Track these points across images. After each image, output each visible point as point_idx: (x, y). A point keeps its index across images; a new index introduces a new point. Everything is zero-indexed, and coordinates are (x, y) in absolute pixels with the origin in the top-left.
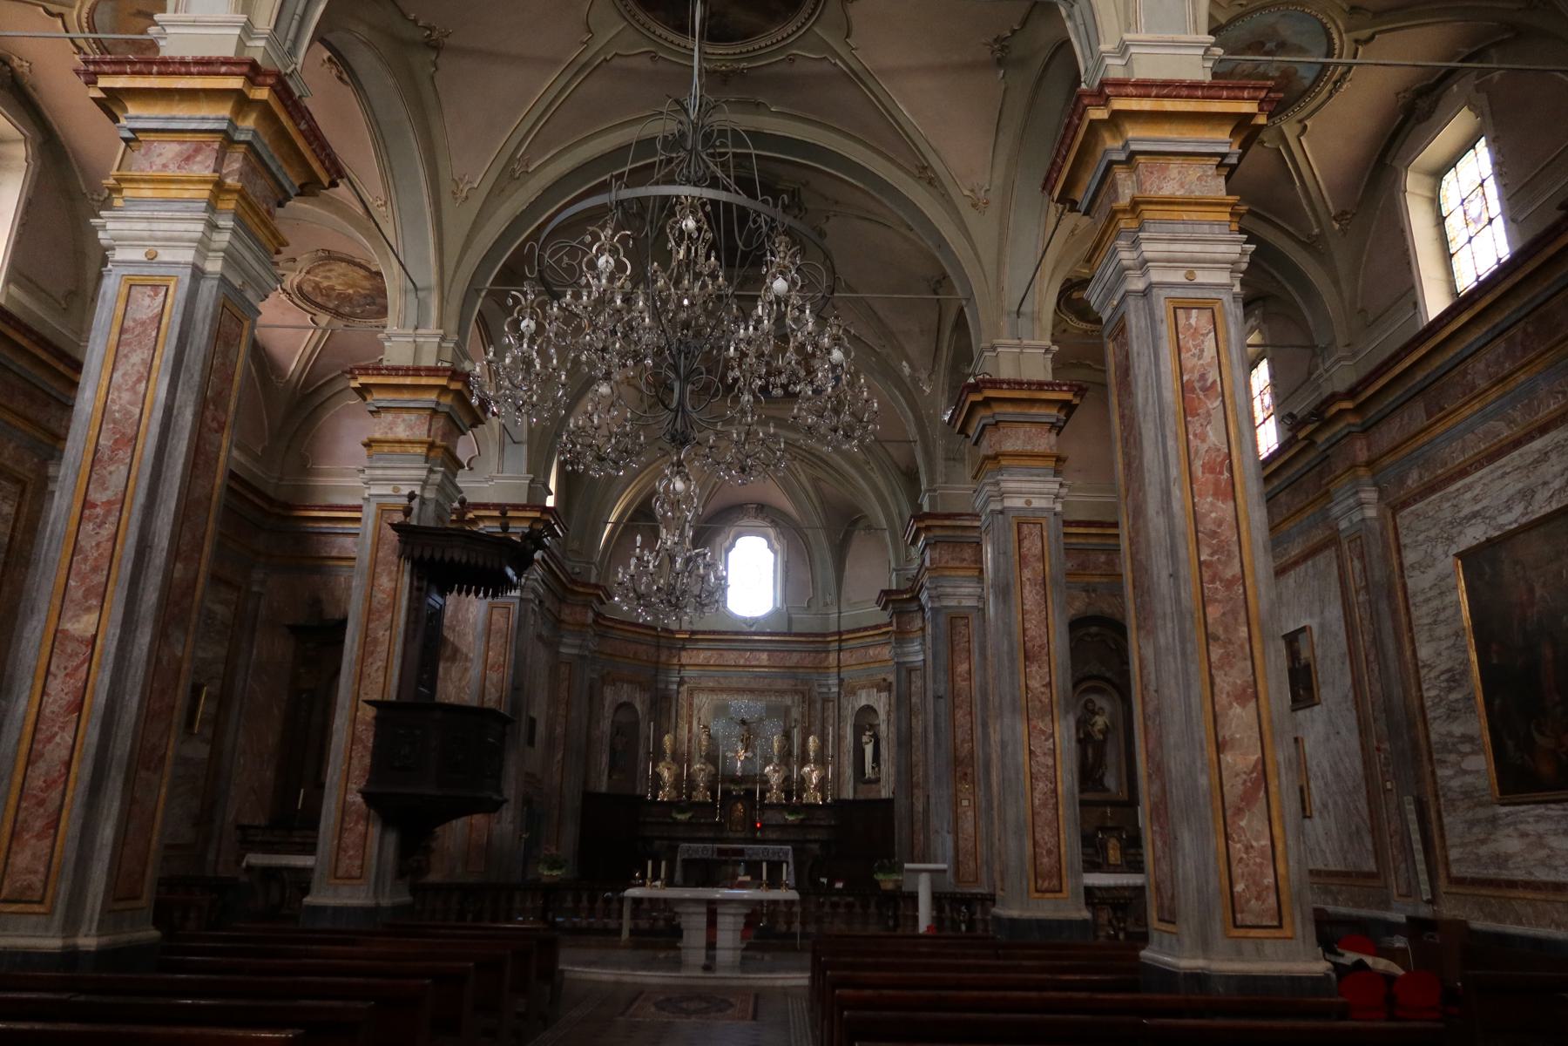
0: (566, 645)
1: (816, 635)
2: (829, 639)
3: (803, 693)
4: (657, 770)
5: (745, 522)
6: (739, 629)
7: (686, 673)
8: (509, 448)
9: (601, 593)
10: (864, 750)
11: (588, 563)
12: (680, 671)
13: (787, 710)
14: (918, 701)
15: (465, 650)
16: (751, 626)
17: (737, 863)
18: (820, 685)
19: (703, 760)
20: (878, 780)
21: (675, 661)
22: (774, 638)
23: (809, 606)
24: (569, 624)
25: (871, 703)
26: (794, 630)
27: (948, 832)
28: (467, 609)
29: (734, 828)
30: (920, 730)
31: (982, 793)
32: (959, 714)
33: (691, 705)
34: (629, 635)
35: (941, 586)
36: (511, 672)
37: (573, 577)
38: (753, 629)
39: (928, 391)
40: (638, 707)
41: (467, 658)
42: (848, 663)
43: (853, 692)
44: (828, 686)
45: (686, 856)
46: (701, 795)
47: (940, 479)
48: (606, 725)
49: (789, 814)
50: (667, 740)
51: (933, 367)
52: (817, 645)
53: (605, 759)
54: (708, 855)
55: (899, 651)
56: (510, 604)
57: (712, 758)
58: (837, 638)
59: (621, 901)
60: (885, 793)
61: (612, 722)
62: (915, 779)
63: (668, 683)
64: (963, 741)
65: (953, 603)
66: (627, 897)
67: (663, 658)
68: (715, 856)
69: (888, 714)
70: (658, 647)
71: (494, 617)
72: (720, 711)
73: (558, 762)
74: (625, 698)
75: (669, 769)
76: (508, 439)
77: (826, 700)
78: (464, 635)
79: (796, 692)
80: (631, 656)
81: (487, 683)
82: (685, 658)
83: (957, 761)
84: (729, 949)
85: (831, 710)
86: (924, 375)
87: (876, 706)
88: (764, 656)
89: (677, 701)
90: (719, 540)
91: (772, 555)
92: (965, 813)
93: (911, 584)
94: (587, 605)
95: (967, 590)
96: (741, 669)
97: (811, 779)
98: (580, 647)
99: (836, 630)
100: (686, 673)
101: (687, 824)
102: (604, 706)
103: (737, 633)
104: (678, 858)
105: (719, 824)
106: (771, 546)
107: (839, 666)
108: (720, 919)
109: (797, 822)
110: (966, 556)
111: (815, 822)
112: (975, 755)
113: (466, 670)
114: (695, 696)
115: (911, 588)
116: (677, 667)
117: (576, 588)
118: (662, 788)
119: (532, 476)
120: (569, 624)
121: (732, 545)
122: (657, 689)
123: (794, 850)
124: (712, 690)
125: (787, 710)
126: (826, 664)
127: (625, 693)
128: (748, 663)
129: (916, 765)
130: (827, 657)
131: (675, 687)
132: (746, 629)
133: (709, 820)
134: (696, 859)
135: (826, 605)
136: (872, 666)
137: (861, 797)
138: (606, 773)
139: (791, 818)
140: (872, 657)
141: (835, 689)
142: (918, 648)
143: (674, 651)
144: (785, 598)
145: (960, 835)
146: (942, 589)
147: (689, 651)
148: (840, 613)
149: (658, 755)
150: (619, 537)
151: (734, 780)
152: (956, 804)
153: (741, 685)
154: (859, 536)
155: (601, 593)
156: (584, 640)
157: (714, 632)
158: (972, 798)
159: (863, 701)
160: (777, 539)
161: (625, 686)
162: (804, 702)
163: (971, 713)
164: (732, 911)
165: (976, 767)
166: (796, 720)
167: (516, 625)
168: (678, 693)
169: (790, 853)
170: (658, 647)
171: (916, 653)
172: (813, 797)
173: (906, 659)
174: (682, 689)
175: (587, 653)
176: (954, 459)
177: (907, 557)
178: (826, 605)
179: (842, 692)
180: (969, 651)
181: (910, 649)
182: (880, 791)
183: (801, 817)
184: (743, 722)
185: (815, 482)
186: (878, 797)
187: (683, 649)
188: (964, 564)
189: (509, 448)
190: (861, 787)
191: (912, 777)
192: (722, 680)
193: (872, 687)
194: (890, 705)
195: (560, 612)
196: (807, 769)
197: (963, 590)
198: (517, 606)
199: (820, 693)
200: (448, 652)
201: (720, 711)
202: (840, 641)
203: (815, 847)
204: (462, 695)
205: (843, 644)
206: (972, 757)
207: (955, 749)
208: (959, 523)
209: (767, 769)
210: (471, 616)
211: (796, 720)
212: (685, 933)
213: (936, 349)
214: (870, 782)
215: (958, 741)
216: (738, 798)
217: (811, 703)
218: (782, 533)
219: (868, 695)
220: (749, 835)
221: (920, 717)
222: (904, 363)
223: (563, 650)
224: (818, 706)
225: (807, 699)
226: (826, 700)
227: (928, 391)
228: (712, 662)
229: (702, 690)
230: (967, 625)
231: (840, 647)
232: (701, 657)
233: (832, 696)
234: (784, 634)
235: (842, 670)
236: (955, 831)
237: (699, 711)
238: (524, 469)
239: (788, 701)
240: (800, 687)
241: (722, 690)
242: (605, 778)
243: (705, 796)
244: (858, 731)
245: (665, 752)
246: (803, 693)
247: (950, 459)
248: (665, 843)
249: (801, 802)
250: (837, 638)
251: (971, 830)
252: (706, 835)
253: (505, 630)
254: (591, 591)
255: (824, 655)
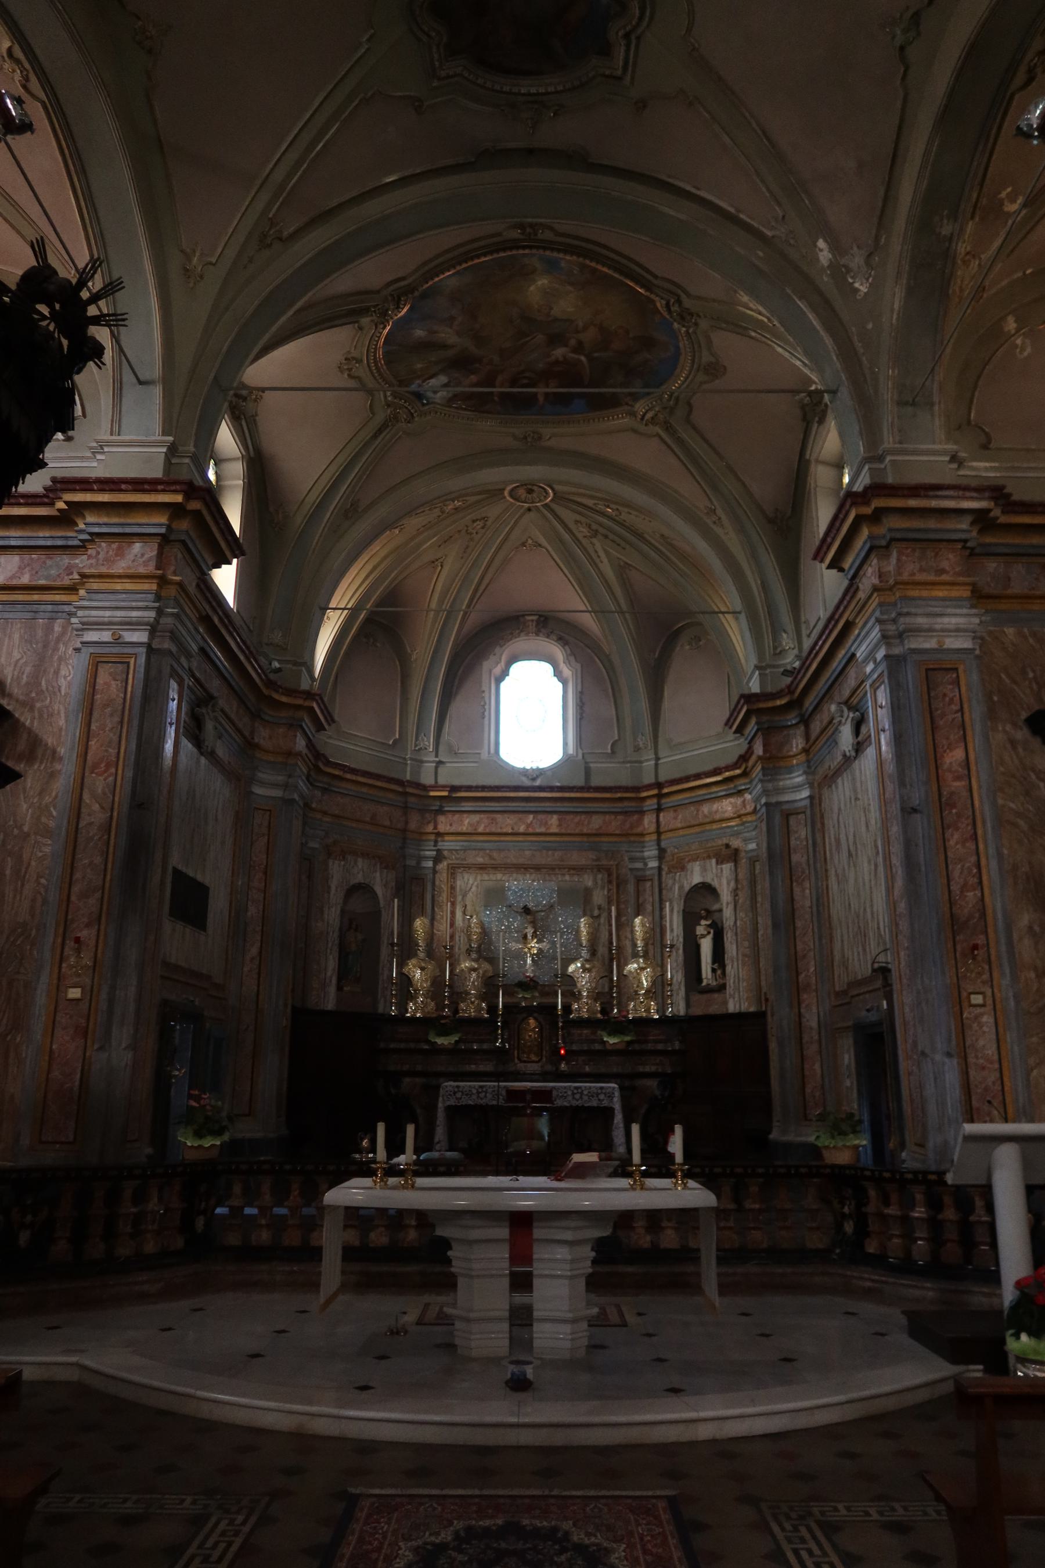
0: (263, 784)
1: (626, 789)
2: (645, 794)
3: (609, 871)
4: (405, 970)
5: (520, 643)
6: (520, 784)
7: (448, 844)
8: (132, 393)
9: (315, 705)
10: (698, 947)
11: (295, 664)
12: (436, 842)
13: (588, 893)
14: (804, 860)
15: (50, 741)
16: (534, 779)
17: (538, 1113)
18: (632, 859)
19: (474, 956)
20: (722, 988)
21: (430, 828)
22: (567, 795)
23: (613, 752)
24: (266, 751)
25: (708, 880)
26: (595, 782)
27: (949, 1055)
28: (57, 672)
29: (524, 1057)
30: (808, 903)
31: (1006, 981)
32: (954, 839)
33: (453, 888)
34: (365, 790)
35: (908, 614)
36: (130, 774)
37: (272, 676)
38: (538, 783)
39: (864, 289)
40: (379, 890)
41: (54, 756)
42: (671, 826)
43: (681, 866)
44: (643, 860)
45: (452, 1102)
46: (470, 1009)
47: (888, 441)
48: (332, 916)
49: (610, 1035)
50: (420, 925)
51: (877, 239)
52: (626, 804)
53: (331, 965)
54: (489, 1100)
55: (770, 786)
56: (130, 655)
57: (484, 951)
58: (655, 792)
59: (322, 1209)
60: (736, 1002)
61: (343, 912)
62: (802, 977)
63: (420, 859)
64: (964, 888)
65: (931, 644)
66: (334, 1208)
67: (413, 825)
68: (502, 1102)
69: (735, 892)
70: (406, 808)
71: (100, 681)
72: (494, 896)
73: (252, 959)
74: (359, 878)
75: (422, 969)
76: (128, 377)
77: (640, 880)
78: (51, 715)
79: (599, 869)
80: (368, 819)
81: (86, 797)
82: (444, 824)
83: (955, 924)
84: (564, 1321)
85: (648, 892)
86: (857, 260)
87: (715, 884)
88: (554, 820)
89: (434, 883)
90: (486, 665)
91: (560, 685)
92: (977, 1017)
93: (789, 680)
94: (295, 725)
95: (954, 620)
96: (521, 838)
97: (640, 982)
98: (286, 786)
99: (652, 780)
100: (448, 844)
101: (452, 1051)
102: (329, 887)
103: (517, 788)
104: (440, 1105)
105: (502, 1050)
106: (558, 674)
107: (659, 833)
108: (540, 1253)
109: (622, 1047)
110: (945, 564)
111: (650, 1046)
112: (989, 912)
113: (53, 775)
114: (459, 877)
115: (789, 687)
116: (433, 837)
117: (276, 696)
118: (413, 998)
119: (171, 438)
120: (266, 751)
121: (505, 673)
122: (405, 866)
123: (622, 1088)
124: (482, 868)
125: (588, 893)
126: (639, 830)
127: (360, 871)
128: (530, 830)
129: (804, 956)
130: (640, 821)
131: (430, 864)
132: (527, 782)
133: (485, 1046)
134: (468, 1106)
135: (637, 749)
136: (708, 827)
137: (697, 1011)
138: (334, 981)
139: (612, 1040)
140: (706, 816)
141: (653, 864)
142: (799, 779)
143: (427, 815)
144: (580, 740)
145: (971, 1060)
146: (908, 620)
147: (450, 815)
148: (657, 759)
149: (406, 949)
150: (347, 654)
151: (528, 985)
152: (959, 1002)
153: (521, 861)
154: (683, 648)
155: (315, 705)
156: (290, 776)
157: (483, 788)
158: (989, 993)
159: (696, 876)
160: (567, 661)
161: (360, 860)
162: (610, 882)
163: (975, 837)
164: (568, 1236)
165: (991, 935)
166: (600, 908)
167: (139, 692)
168: (435, 872)
169: (617, 1094)
170: (406, 808)
171: (798, 788)
172: (638, 1009)
173: (786, 798)
174: (440, 867)
175: (296, 796)
176: (914, 404)
177: (775, 648)
178: (637, 749)
179: (665, 868)
180: (963, 726)
181: (788, 782)
182: (725, 1003)
183: (628, 1038)
184: (526, 910)
185: (622, 570)
186: (724, 1011)
187: (440, 811)
188: (945, 577)
189: (132, 393)
190: (696, 997)
191: (798, 974)
192: (495, 854)
193: (709, 857)
194: (737, 881)
195: (252, 733)
196: (633, 966)
197: (946, 620)
198: (142, 660)
199: (631, 870)
200: (22, 745)
201: (494, 896)
202: (660, 796)
203: (653, 1084)
204: (44, 820)
205: (663, 801)
206: (983, 915)
207: (951, 903)
208: (934, 503)
209: (571, 968)
210: (63, 683)
211: (600, 908)
212: (461, 1282)
213: (886, 199)
214: (709, 990)
215: (955, 888)
216: (530, 1011)
217: (621, 883)
218: (573, 654)
219: (704, 870)
220: (549, 1068)
221: (807, 884)
222: (821, 244)
223: (258, 790)
224: (631, 888)
225: (616, 881)
226: (640, 880)
227: (864, 289)
228: (480, 830)
229: (468, 867)
230: (957, 682)
231: (659, 804)
232: (466, 823)
233: (648, 873)
234: (581, 789)
235: (663, 837)
236: (962, 1053)
237: (464, 896)
238: (157, 426)
239: (588, 881)
240: (604, 862)
241: (495, 868)
242: (332, 990)
243: (479, 1009)
244: (690, 920)
245: (417, 945)
246: (609, 871)
247: (906, 403)
248: (419, 1080)
249: (626, 1017)
250: (655, 792)
251: (991, 1051)
252: (482, 1068)
253: (120, 701)
254: (300, 702)
255: (636, 817)
